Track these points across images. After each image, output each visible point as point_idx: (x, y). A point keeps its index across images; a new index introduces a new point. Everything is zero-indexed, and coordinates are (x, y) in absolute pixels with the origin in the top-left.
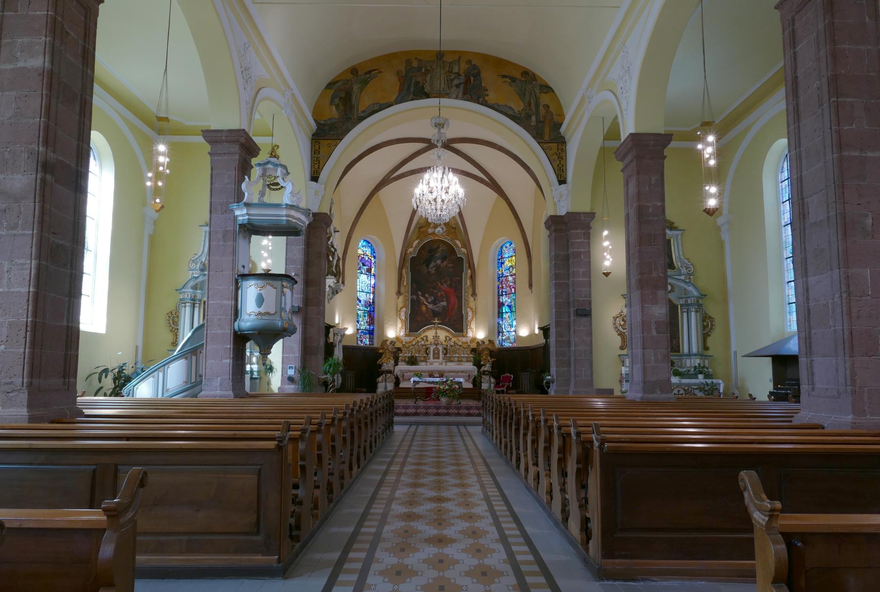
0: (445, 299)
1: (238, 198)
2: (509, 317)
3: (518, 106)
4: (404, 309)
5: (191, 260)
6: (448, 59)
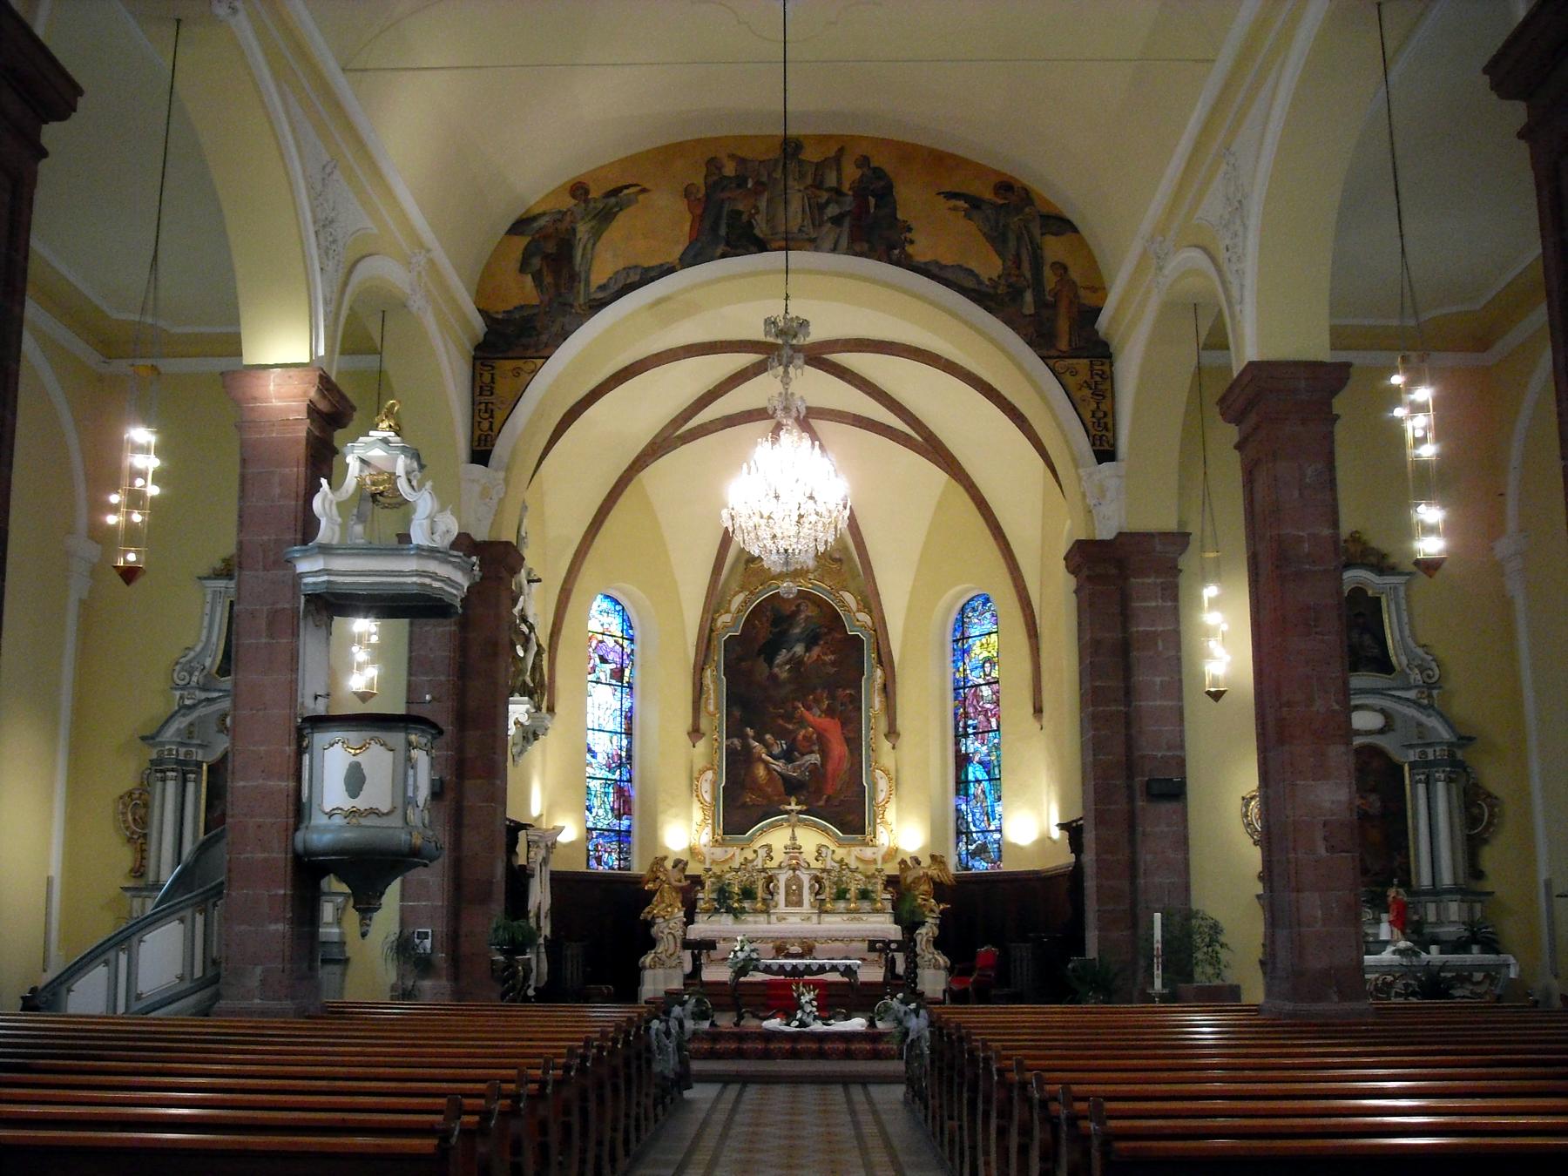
0: (816, 748)
1: (304, 534)
2: (984, 792)
3: (988, 266)
4: (709, 775)
5: (177, 663)
6: (811, 155)
